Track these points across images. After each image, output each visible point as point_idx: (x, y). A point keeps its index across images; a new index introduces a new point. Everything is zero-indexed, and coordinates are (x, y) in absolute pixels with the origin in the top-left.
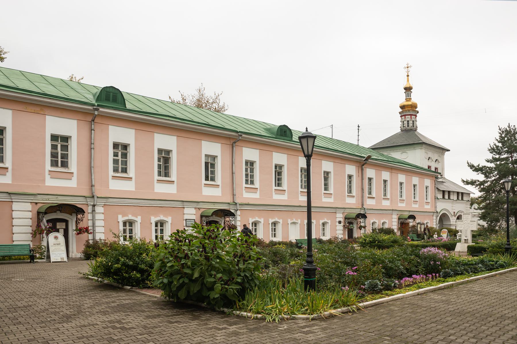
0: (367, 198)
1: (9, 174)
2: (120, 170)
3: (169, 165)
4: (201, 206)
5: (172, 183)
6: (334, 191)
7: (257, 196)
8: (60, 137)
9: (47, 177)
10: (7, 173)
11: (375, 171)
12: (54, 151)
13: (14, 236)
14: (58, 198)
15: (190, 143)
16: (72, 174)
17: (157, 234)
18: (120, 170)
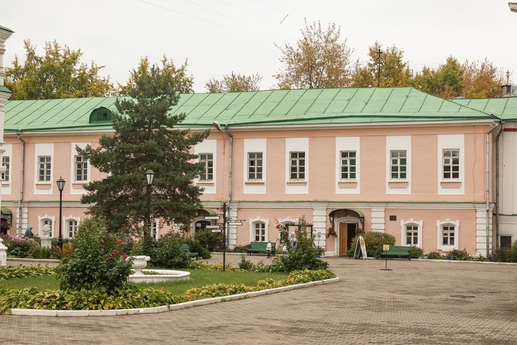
0: (244, 184)
1: (463, 187)
2: (298, 176)
3: (76, 169)
4: (390, 206)
5: (354, 185)
6: (217, 180)
7: (408, 191)
8: (47, 158)
9: (387, 187)
10: (440, 221)
11: (465, 138)
12: (79, 169)
13: (477, 238)
14: (312, 205)
15: (322, 142)
16: (356, 184)
17: (258, 235)
18: (298, 176)
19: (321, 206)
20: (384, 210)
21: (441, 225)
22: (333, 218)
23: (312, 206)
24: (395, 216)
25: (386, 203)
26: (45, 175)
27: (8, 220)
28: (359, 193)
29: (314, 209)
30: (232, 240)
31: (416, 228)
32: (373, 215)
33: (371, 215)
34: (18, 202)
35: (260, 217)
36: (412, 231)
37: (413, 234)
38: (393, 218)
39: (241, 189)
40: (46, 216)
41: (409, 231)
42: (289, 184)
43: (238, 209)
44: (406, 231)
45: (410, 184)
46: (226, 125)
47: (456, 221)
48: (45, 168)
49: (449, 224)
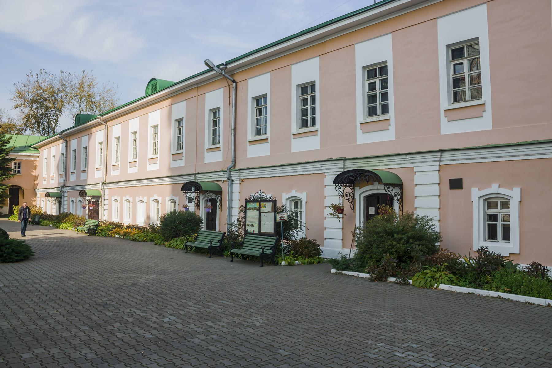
5: (265, 141)
9: (444, 120)
19: (335, 168)
20: (437, 168)
21: (480, 198)
22: (353, 189)
23: (323, 169)
24: (461, 180)
25: (439, 154)
26: (379, 103)
27: (395, 196)
28: (394, 139)
29: (326, 174)
30: (22, 192)
31: (505, 205)
32: (418, 179)
33: (413, 180)
34: (99, 184)
35: (498, 185)
36: (499, 211)
37: (500, 218)
38: (456, 184)
39: (245, 151)
40: (293, 191)
41: (492, 211)
42: (252, 143)
43: (242, 180)
44: (484, 212)
45: (489, 107)
46: (225, 64)
47: (514, 188)
48: (378, 90)
49: (497, 196)
